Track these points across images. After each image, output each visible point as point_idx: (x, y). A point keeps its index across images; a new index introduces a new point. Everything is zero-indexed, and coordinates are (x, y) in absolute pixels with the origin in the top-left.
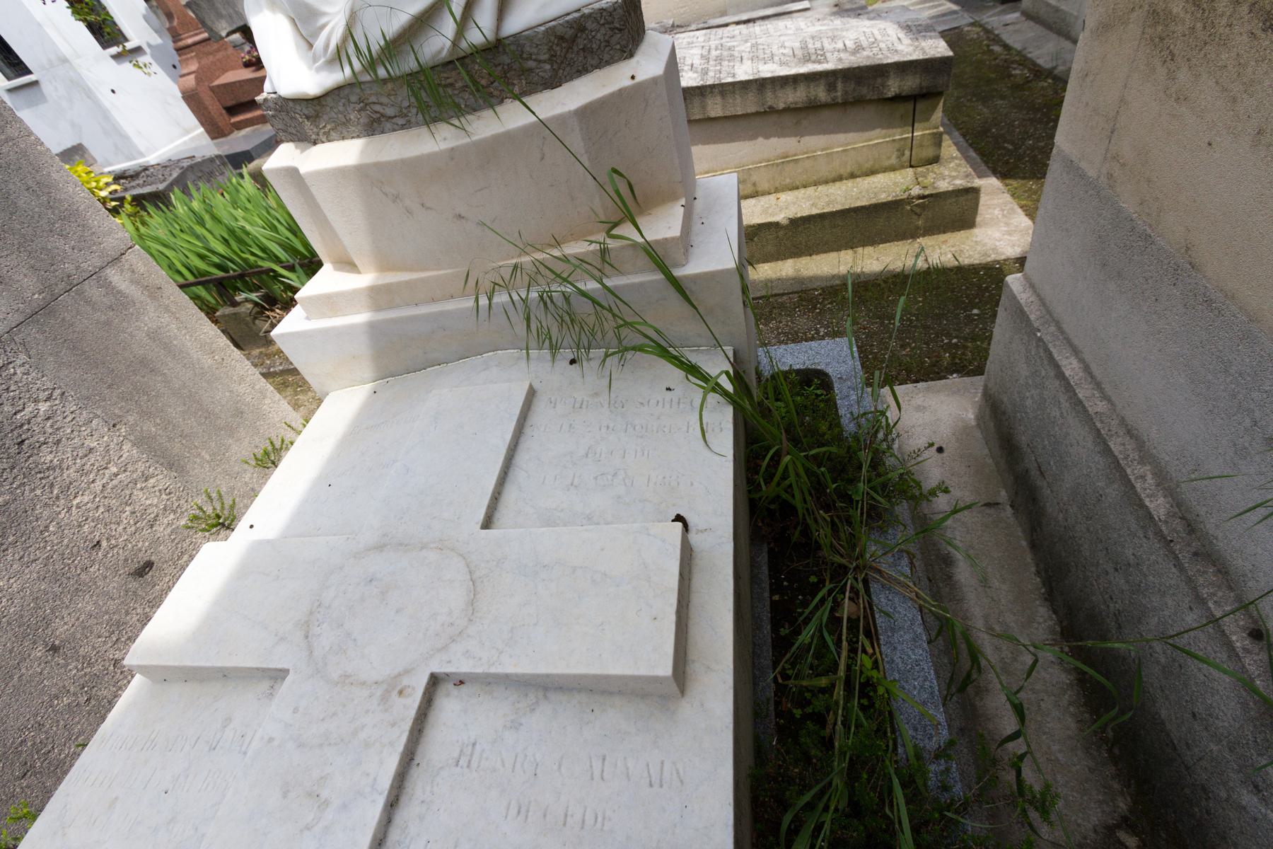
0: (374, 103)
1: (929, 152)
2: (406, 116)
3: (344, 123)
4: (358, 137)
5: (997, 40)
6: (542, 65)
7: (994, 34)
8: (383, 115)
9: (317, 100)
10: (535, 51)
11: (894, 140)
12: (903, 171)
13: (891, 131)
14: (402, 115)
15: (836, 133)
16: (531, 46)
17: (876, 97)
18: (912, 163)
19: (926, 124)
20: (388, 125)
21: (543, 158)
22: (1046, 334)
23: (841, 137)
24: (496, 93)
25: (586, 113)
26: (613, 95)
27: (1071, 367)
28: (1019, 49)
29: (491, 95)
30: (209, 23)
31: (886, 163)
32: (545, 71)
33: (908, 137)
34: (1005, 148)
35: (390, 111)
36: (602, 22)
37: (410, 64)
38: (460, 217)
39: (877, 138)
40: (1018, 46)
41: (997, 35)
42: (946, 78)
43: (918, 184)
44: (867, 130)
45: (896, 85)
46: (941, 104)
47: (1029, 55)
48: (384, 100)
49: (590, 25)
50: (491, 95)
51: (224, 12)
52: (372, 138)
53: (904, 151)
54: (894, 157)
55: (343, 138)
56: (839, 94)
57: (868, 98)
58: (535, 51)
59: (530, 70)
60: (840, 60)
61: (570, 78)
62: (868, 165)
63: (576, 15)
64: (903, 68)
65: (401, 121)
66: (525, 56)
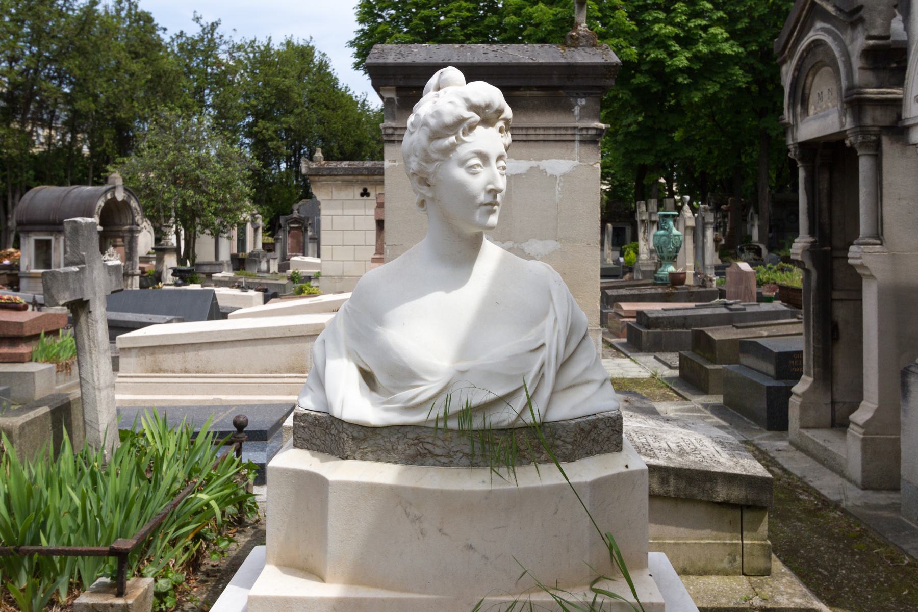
0: (428, 443)
1: (761, 563)
2: (451, 457)
3: (388, 450)
4: (396, 462)
6: (566, 445)
7: (769, 456)
8: (430, 452)
9: (374, 429)
10: (565, 435)
11: (725, 544)
12: (736, 577)
13: (721, 534)
14: (448, 456)
15: (668, 524)
16: (563, 432)
17: (705, 499)
18: (745, 571)
19: (754, 534)
20: (431, 461)
21: (556, 513)
23: (672, 530)
24: (528, 456)
25: (597, 485)
26: (613, 476)
28: (799, 476)
29: (524, 457)
30: (54, 291)
31: (720, 566)
32: (567, 449)
33: (738, 544)
34: (820, 573)
35: (438, 451)
36: (608, 425)
37: (477, 424)
38: (470, 547)
39: (708, 538)
40: (798, 473)
41: (773, 458)
42: (769, 496)
43: (757, 595)
44: (698, 528)
45: (724, 492)
47: (811, 484)
48: (439, 443)
49: (601, 425)
50: (524, 457)
51: (72, 286)
52: (409, 467)
53: (735, 556)
54: (726, 560)
55: (378, 460)
56: (672, 489)
57: (699, 498)
58: (565, 435)
59: (557, 446)
60: (669, 458)
61: (581, 457)
62: (700, 564)
63: (594, 417)
64: (730, 479)
65: (443, 460)
66: (556, 436)
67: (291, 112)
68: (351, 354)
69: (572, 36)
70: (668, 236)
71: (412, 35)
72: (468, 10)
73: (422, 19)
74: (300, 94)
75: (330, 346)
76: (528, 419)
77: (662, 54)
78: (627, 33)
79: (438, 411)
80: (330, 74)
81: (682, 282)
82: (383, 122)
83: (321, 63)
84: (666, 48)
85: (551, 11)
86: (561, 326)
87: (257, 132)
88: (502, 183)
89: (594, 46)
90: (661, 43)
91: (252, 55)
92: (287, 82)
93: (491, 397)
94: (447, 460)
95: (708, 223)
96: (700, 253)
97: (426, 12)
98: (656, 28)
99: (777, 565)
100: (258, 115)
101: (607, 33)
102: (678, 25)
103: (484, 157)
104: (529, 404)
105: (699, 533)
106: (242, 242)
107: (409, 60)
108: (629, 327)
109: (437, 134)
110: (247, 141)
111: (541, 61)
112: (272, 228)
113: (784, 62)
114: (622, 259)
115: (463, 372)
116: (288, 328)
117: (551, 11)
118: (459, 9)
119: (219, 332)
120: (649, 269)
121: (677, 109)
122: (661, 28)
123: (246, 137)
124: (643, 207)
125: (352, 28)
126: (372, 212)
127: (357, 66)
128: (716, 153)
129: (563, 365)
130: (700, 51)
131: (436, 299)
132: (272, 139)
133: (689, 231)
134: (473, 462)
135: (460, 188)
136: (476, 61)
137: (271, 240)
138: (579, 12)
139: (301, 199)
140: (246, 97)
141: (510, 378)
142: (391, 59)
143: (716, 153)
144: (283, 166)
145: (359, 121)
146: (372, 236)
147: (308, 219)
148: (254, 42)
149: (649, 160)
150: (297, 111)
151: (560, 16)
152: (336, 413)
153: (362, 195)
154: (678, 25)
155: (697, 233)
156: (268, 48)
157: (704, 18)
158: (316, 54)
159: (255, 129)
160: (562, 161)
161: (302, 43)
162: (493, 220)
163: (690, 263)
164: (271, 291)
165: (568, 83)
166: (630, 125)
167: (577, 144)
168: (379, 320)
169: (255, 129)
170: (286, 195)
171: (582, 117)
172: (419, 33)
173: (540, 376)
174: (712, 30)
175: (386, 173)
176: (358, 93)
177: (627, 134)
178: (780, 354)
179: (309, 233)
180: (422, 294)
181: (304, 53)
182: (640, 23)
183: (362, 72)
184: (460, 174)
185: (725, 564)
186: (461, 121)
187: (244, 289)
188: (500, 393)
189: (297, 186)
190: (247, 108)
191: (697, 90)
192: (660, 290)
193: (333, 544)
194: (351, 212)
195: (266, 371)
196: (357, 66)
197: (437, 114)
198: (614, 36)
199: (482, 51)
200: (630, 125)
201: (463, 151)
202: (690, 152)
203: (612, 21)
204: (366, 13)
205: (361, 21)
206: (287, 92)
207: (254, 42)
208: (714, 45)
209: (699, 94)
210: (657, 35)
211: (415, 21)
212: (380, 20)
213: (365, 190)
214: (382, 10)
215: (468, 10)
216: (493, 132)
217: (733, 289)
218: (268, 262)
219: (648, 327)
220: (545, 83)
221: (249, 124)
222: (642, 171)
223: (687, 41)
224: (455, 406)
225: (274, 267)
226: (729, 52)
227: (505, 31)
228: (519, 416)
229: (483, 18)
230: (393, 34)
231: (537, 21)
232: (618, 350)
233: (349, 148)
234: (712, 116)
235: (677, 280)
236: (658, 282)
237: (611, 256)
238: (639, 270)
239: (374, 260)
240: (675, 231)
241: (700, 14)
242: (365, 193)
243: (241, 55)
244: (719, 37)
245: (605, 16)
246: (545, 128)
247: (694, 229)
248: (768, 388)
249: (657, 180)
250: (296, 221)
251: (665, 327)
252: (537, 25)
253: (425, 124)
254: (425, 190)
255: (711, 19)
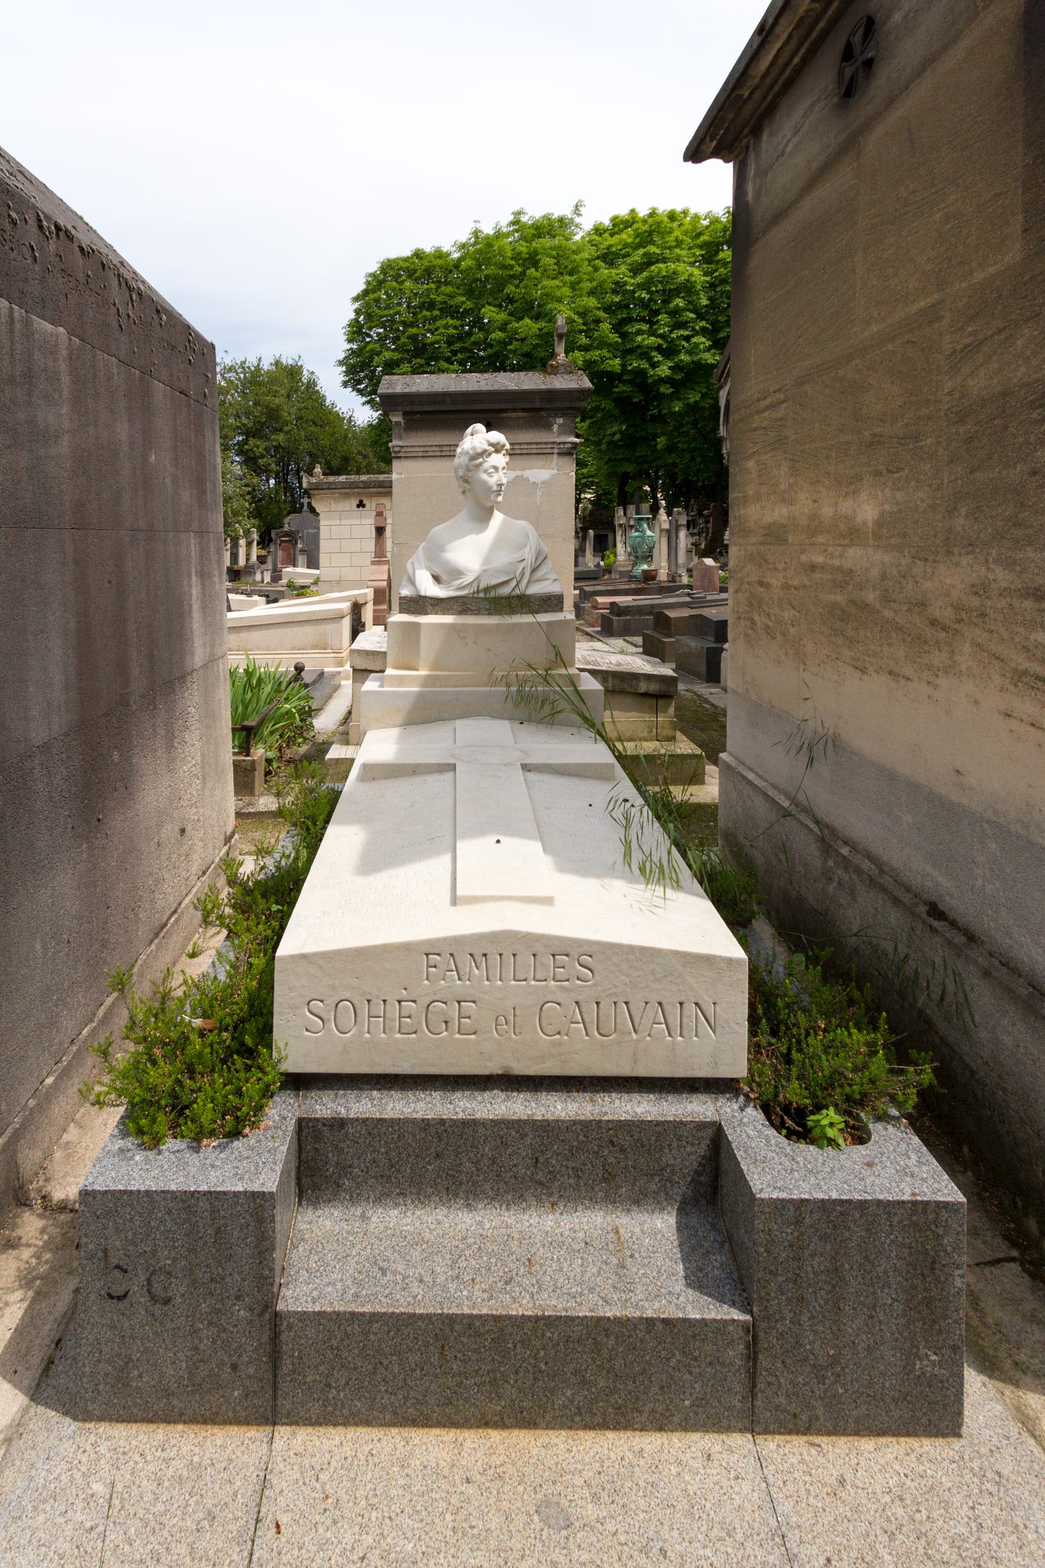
1: (669, 733)
5: (706, 701)
13: (642, 715)
22: (740, 769)
25: (550, 624)
27: (751, 776)
31: (642, 735)
37: (492, 594)
46: (673, 704)
64: (649, 677)
67: (281, 430)
68: (428, 568)
69: (552, 365)
70: (642, 537)
71: (400, 353)
72: (455, 328)
73: (409, 337)
74: (289, 413)
75: (416, 565)
76: (517, 592)
77: (644, 365)
78: (610, 345)
79: (474, 588)
80: (318, 392)
81: (654, 578)
82: (391, 441)
83: (309, 382)
84: (649, 359)
85: (537, 326)
86: (533, 551)
87: (248, 450)
88: (504, 481)
89: (571, 373)
90: (645, 355)
91: (242, 376)
92: (277, 401)
93: (500, 581)
94: (478, 612)
95: (681, 525)
96: (673, 553)
97: (413, 331)
98: (639, 338)
99: (679, 736)
100: (248, 433)
101: (591, 345)
102: (662, 336)
103: (496, 468)
104: (517, 585)
105: (628, 714)
106: (234, 557)
107: (414, 389)
108: (603, 616)
109: (473, 458)
110: (237, 459)
111: (525, 388)
112: (265, 541)
113: (721, 387)
114: (602, 563)
115: (485, 571)
116: (313, 613)
117: (537, 326)
118: (446, 327)
119: (257, 617)
120: (626, 569)
121: (660, 419)
122: (644, 339)
123: (237, 455)
124: (620, 512)
125: (341, 347)
126: (372, 521)
127: (345, 384)
128: (698, 459)
129: (534, 571)
130: (681, 361)
131: (471, 538)
132: (262, 456)
133: (664, 533)
134: (490, 612)
135: (484, 483)
136: (470, 389)
137: (264, 553)
138: (559, 344)
139: (289, 514)
140: (237, 416)
141: (508, 573)
142: (399, 389)
143: (698, 459)
144: (272, 482)
145: (346, 436)
146: (371, 545)
147: (298, 532)
148: (244, 362)
149: (630, 468)
150: (286, 429)
151: (545, 330)
152: (423, 594)
153: (358, 506)
154: (662, 336)
155: (671, 535)
156: (258, 368)
157: (686, 329)
158: (305, 372)
159: (246, 447)
160: (543, 471)
161: (290, 362)
162: (500, 499)
163: (664, 564)
164: (272, 598)
165: (548, 406)
166: (614, 434)
167: (555, 456)
168: (442, 549)
169: (246, 447)
170: (276, 511)
171: (560, 434)
172: (407, 351)
173: (523, 574)
174: (694, 340)
175: (394, 484)
176: (344, 410)
177: (609, 443)
178: (718, 622)
179: (300, 546)
180: (464, 536)
181: (293, 372)
182: (624, 335)
183: (350, 389)
184: (484, 476)
185: (645, 734)
186: (485, 451)
187: (249, 595)
188: (505, 579)
189: (285, 501)
190: (238, 427)
191: (679, 399)
192: (633, 586)
193: (423, 653)
194: (349, 522)
195: (294, 648)
196: (345, 384)
197: (474, 448)
198: (597, 348)
199: (475, 380)
200: (614, 434)
201: (486, 465)
202: (671, 459)
203: (596, 334)
204: (354, 333)
205: (350, 341)
206: (277, 411)
207: (244, 362)
208: (697, 354)
209: (680, 404)
210: (639, 347)
211: (403, 340)
212: (368, 339)
213: (361, 501)
214: (370, 329)
215: (455, 328)
216: (500, 456)
217: (698, 583)
218: (262, 573)
219: (619, 615)
220: (529, 406)
221: (238, 443)
222: (624, 478)
223: (669, 351)
224: (482, 586)
225: (267, 578)
226: (711, 361)
227: (491, 346)
228: (513, 589)
229: (469, 334)
230: (381, 352)
231: (523, 335)
232: (592, 636)
233: (336, 463)
234: (695, 424)
235: (649, 576)
236: (631, 578)
237: (591, 561)
238: (616, 571)
239: (373, 563)
240: (649, 533)
241: (683, 325)
242: (361, 505)
243: (231, 376)
244: (702, 347)
245: (589, 330)
246: (528, 444)
247: (668, 531)
248: (708, 648)
249: (640, 488)
250: (287, 534)
251: (634, 614)
252: (523, 340)
253: (467, 453)
254: (466, 485)
255: (693, 329)
